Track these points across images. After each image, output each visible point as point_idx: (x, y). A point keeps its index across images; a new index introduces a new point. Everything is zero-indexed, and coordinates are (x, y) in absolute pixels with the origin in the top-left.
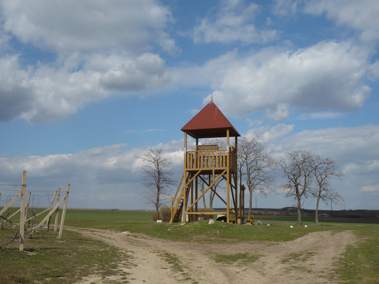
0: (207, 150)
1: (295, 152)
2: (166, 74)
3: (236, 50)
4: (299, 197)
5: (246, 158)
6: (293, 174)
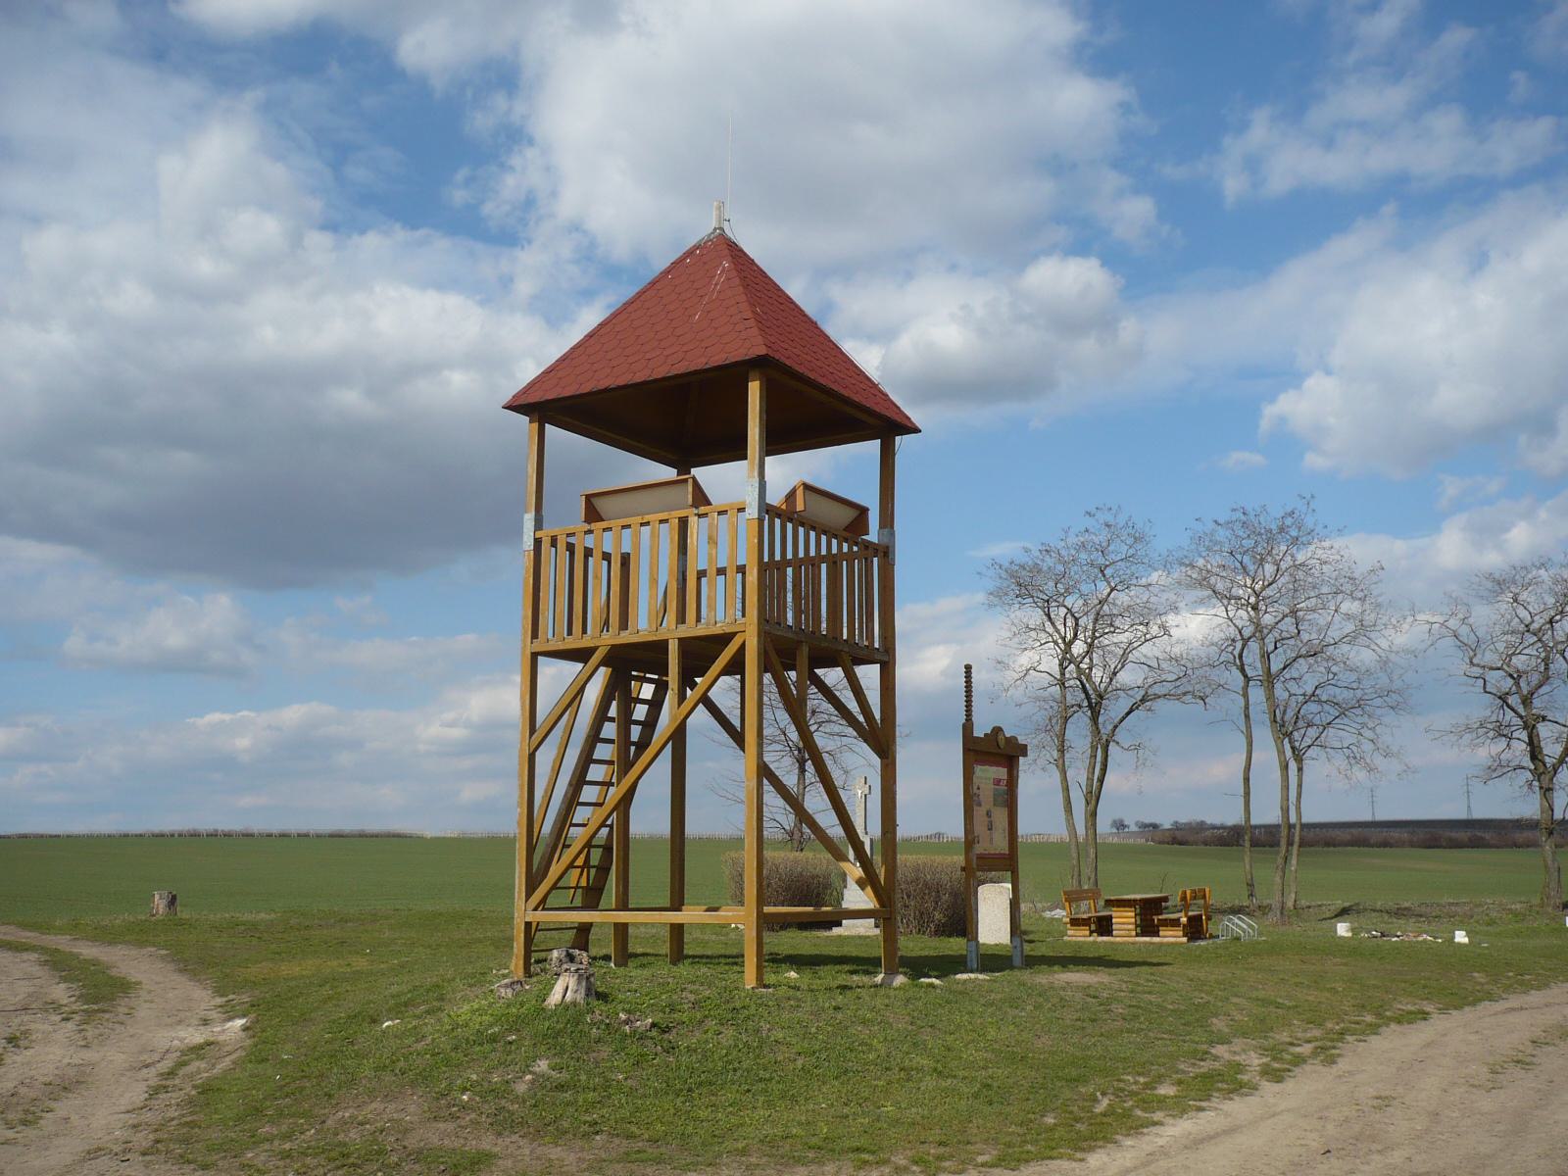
0: (639, 519)
1: (1515, 568)
2: (1129, 329)
3: (1389, 209)
4: (1545, 779)
6: (1511, 671)
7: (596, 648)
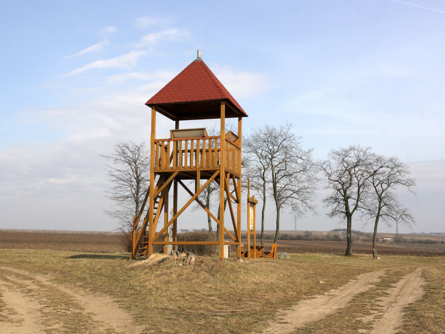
5: (271, 158)
7: (174, 172)
